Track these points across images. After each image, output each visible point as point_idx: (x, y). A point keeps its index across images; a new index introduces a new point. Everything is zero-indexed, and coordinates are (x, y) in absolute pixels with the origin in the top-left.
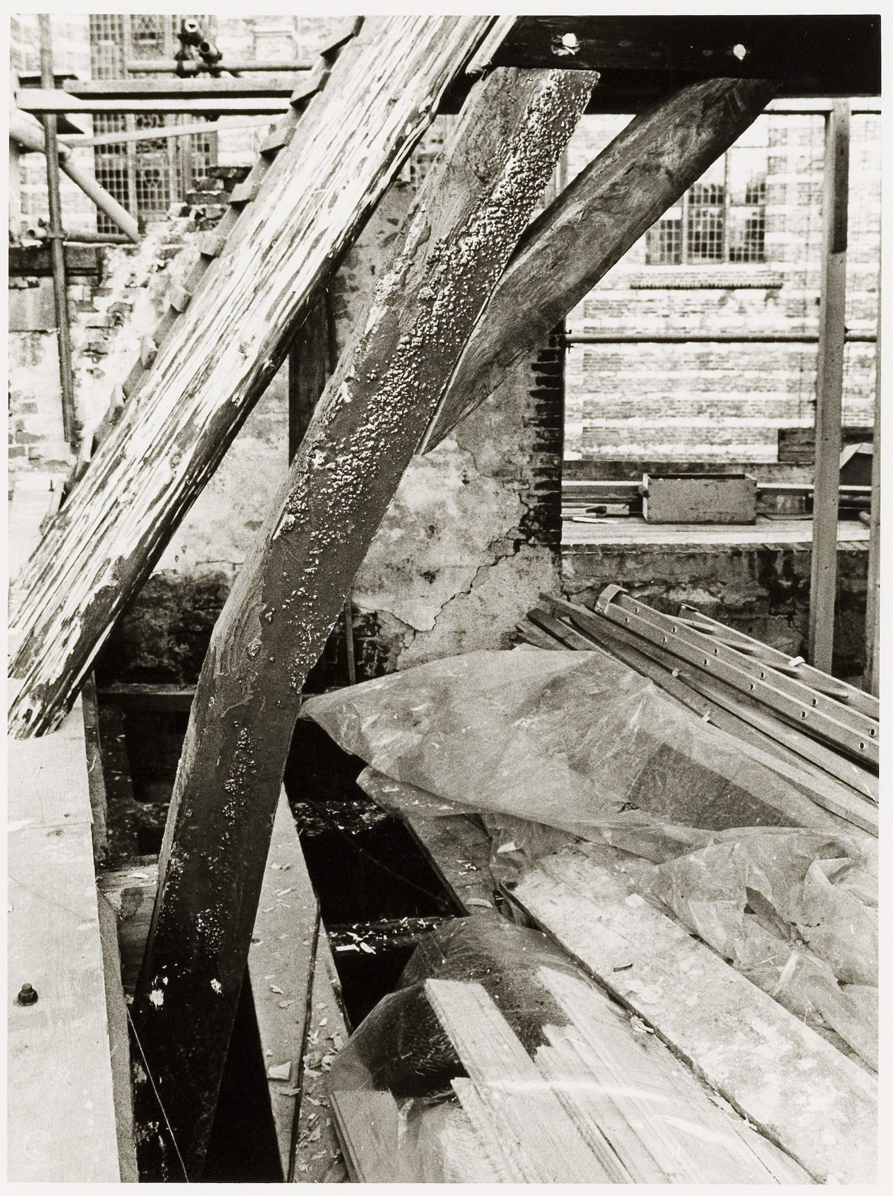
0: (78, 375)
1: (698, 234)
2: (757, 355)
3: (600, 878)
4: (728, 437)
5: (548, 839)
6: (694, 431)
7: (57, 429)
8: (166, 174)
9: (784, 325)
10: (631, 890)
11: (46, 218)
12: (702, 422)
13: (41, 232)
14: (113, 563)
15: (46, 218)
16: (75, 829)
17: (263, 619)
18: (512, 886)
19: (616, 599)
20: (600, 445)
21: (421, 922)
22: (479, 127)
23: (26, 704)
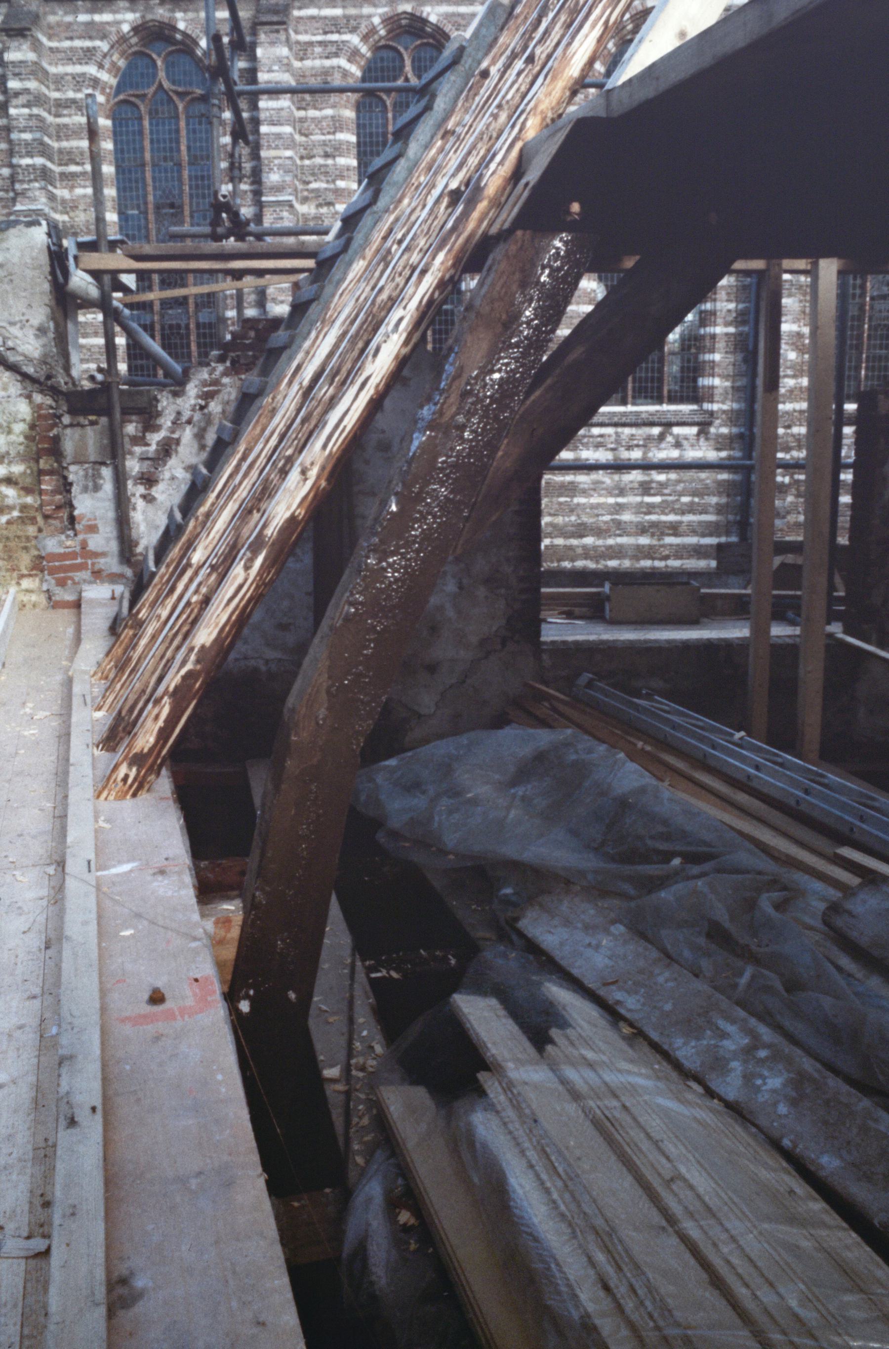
0: (133, 500)
1: (640, 378)
2: (691, 483)
3: (588, 912)
4: (667, 552)
5: (540, 882)
6: (639, 547)
7: (114, 546)
8: (187, 327)
9: (712, 455)
10: (613, 922)
11: (104, 365)
12: (644, 540)
13: (100, 377)
14: (196, 650)
15: (104, 365)
16: (177, 869)
17: (328, 692)
18: (517, 919)
19: (589, 685)
20: (559, 561)
21: (438, 953)
22: (502, 281)
23: (123, 770)
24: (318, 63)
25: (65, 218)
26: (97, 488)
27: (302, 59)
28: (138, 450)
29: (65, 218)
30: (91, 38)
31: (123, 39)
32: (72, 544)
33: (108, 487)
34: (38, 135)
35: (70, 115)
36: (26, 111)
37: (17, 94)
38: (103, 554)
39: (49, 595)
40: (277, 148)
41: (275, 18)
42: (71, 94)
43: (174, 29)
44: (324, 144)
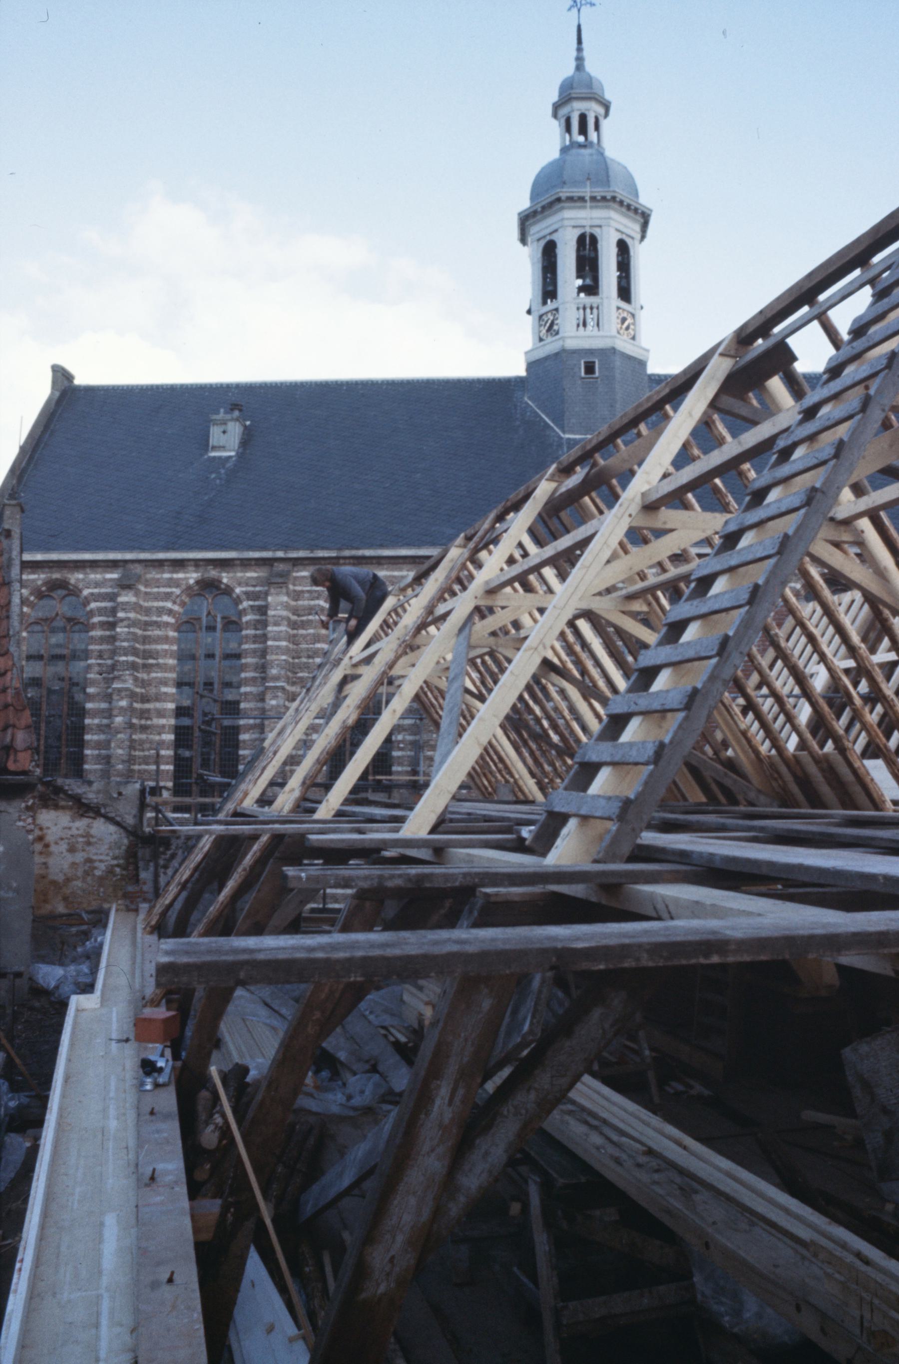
7: (152, 890)
24: (306, 603)
25: (143, 691)
26: (148, 869)
27: (296, 600)
28: (163, 856)
29: (143, 691)
30: (170, 587)
31: (189, 588)
32: (137, 888)
33: (152, 869)
34: (132, 644)
35: (152, 630)
36: (126, 630)
37: (122, 620)
38: (147, 893)
39: (127, 906)
40: (277, 654)
41: (280, 580)
42: (155, 618)
43: (220, 582)
44: (308, 650)
